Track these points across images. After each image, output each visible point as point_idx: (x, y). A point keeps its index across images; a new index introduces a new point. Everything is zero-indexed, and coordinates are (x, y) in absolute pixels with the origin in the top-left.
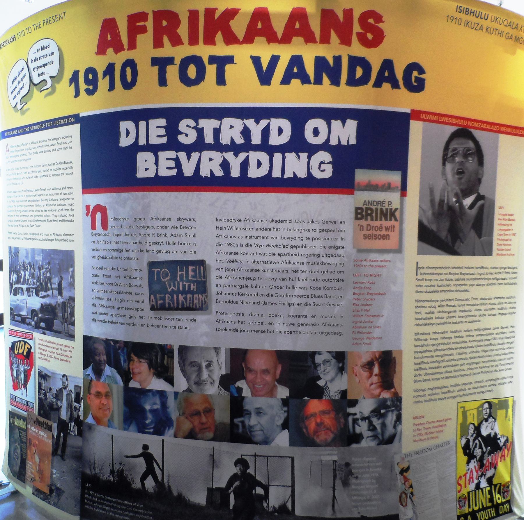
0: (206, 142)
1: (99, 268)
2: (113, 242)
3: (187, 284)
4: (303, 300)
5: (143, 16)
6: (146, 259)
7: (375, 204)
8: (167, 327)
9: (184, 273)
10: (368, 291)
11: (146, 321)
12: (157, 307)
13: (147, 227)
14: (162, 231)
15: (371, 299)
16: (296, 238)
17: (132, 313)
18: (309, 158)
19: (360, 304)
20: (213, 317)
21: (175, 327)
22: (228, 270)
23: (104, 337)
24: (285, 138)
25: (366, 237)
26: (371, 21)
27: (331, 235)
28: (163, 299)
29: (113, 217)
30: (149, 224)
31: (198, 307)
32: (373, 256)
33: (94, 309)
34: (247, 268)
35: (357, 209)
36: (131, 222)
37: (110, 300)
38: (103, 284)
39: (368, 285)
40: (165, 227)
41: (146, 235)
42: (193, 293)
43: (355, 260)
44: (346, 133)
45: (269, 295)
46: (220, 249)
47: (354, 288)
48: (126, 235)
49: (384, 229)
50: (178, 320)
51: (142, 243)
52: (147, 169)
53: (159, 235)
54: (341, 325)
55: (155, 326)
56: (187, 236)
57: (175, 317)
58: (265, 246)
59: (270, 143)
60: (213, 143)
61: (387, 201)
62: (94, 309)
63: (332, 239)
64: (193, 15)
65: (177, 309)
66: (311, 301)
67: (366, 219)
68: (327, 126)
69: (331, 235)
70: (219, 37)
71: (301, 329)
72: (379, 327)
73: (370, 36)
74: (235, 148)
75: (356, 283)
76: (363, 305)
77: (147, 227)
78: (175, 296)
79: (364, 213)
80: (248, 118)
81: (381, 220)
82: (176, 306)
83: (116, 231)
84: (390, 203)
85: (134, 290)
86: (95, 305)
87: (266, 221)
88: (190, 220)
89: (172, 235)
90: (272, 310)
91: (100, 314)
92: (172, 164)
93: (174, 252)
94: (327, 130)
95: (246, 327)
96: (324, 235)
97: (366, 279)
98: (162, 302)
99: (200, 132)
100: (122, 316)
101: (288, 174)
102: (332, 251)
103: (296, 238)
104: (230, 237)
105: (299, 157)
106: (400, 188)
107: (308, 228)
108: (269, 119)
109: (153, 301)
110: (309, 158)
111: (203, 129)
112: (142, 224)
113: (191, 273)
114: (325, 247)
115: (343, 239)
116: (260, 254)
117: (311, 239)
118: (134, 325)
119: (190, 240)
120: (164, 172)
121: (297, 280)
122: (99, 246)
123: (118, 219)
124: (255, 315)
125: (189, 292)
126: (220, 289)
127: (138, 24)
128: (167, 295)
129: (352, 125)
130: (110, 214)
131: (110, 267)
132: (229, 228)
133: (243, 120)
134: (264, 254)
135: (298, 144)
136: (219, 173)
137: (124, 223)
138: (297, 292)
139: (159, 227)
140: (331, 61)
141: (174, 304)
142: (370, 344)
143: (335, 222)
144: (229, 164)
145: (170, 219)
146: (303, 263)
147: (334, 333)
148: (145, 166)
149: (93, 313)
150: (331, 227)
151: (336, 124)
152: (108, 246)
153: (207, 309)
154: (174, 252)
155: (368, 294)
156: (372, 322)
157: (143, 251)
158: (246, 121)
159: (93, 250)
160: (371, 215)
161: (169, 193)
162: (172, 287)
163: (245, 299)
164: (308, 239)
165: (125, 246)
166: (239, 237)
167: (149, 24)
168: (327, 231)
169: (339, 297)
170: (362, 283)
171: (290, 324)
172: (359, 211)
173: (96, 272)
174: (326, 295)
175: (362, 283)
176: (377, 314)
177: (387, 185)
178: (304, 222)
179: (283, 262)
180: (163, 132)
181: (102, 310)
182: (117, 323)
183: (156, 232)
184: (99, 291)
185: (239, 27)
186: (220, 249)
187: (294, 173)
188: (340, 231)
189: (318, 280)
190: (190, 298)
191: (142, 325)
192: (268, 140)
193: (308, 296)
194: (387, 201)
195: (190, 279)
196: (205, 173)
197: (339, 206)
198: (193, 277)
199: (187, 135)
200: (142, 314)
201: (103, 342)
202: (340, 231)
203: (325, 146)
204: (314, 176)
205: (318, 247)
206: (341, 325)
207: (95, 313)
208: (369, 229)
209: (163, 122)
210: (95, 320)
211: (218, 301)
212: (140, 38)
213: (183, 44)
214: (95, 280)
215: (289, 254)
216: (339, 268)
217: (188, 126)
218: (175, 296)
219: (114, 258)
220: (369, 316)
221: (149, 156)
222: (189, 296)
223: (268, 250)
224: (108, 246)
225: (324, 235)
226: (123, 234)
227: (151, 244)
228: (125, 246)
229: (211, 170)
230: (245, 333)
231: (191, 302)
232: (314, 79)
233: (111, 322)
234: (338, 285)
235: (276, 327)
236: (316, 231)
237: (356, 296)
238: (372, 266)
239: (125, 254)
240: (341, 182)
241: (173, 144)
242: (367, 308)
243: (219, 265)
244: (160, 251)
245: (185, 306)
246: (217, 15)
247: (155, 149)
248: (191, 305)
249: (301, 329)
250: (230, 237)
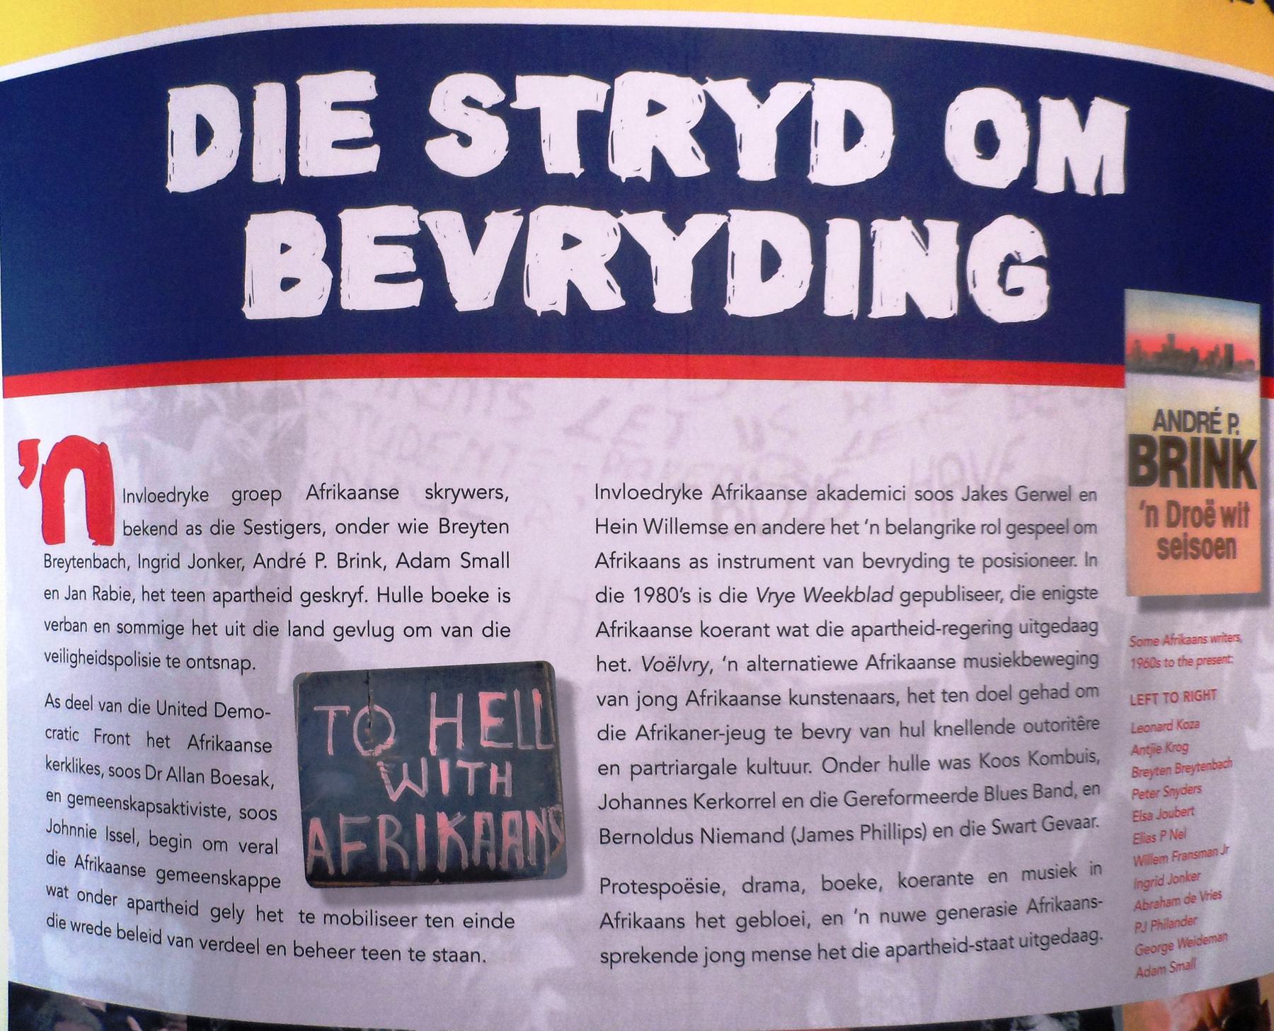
0: (550, 170)
1: (74, 704)
2: (137, 593)
3: (471, 767)
4: (953, 815)
6: (287, 664)
7: (1190, 423)
8: (385, 955)
9: (458, 721)
10: (1178, 757)
11: (289, 931)
12: (338, 869)
13: (292, 530)
14: (354, 545)
15: (1189, 790)
16: (921, 561)
17: (225, 896)
18: (964, 241)
19: (1156, 814)
20: (584, 905)
21: (419, 956)
22: (647, 701)
23: (99, 997)
24: (871, 158)
25: (1170, 550)
27: (1052, 546)
28: (367, 834)
29: (136, 488)
30: (298, 518)
31: (520, 863)
32: (1193, 622)
33: (56, 876)
34: (728, 691)
35: (1136, 441)
36: (219, 504)
37: (126, 838)
38: (92, 770)
39: (1176, 736)
40: (377, 528)
41: (286, 562)
42: (498, 805)
43: (1135, 642)
44: (1089, 148)
45: (824, 801)
46: (612, 613)
47: (1136, 751)
48: (197, 563)
49: (1219, 519)
50: (435, 922)
51: (270, 597)
52: (288, 284)
53: (343, 561)
54: (1094, 903)
55: (331, 953)
56: (468, 562)
57: (424, 910)
58: (800, 597)
59: (815, 177)
60: (578, 171)
61: (1225, 412)
62: (56, 876)
63: (1053, 562)
65: (430, 876)
66: (985, 814)
67: (1165, 483)
68: (1023, 118)
69: (1052, 546)
71: (950, 932)
72: (1217, 896)
74: (669, 195)
75: (1141, 729)
76: (1165, 815)
77: (292, 530)
78: (420, 820)
79: (1157, 459)
80: (723, 74)
81: (1209, 484)
82: (422, 863)
83: (150, 547)
84: (1234, 420)
85: (235, 798)
86: (62, 861)
87: (802, 495)
88: (481, 493)
89: (402, 561)
90: (835, 860)
91: (83, 896)
92: (403, 259)
93: (413, 631)
94: (1025, 134)
95: (727, 939)
96: (1025, 545)
97: (1172, 713)
98: (360, 846)
99: (524, 128)
100: (178, 909)
101: (887, 306)
102: (1053, 611)
103: (921, 561)
104: (656, 564)
105: (924, 234)
106: (1257, 366)
107: (965, 521)
108: (807, 79)
109: (318, 846)
110: (964, 241)
111: (534, 114)
112: (271, 514)
113: (488, 721)
114: (1030, 595)
115: (1091, 560)
116: (783, 632)
117: (978, 565)
118: (237, 947)
119: (481, 579)
120: (363, 295)
121: (930, 730)
122: (74, 611)
123: (160, 497)
124: (768, 888)
125: (482, 800)
126: (613, 786)
128: (382, 819)
129: (1110, 117)
130: (125, 477)
131: (126, 701)
132: (652, 526)
133: (702, 81)
134: (799, 631)
135: (919, 185)
136: (604, 296)
137: (189, 514)
138: (931, 781)
139: (343, 529)
141: (413, 855)
142: (1191, 965)
143: (1063, 496)
144: (647, 258)
145: (392, 494)
146: (950, 664)
147: (1074, 938)
148: (281, 267)
149: (50, 891)
150: (1047, 515)
151: (1057, 112)
152: (118, 612)
153: (560, 868)
154: (413, 631)
155: (1180, 768)
156: (1195, 877)
157: (274, 631)
159: (53, 626)
160: (1176, 465)
161: (389, 383)
162: (406, 783)
163: (725, 820)
164: (967, 562)
165: (190, 613)
166: (695, 563)
168: (1035, 530)
169: (1087, 790)
170: (1160, 728)
171: (907, 917)
172: (1143, 450)
173: (63, 718)
174: (1038, 788)
175: (1160, 728)
176: (1207, 846)
177: (1222, 353)
178: (948, 495)
179: (872, 662)
180: (360, 125)
181: (87, 880)
182: (157, 939)
183: (332, 545)
184: (75, 801)
186: (612, 613)
187: (909, 300)
188: (1082, 529)
189: (1008, 728)
190: (486, 828)
191: (270, 950)
192: (805, 166)
193: (973, 797)
194: (1225, 412)
195: (485, 744)
196: (544, 296)
197: (1070, 432)
198: (495, 734)
199: (465, 140)
200: (269, 899)
201: (92, 1019)
202: (1082, 529)
203: (1021, 198)
205: (1005, 594)
206: (1094, 903)
207: (61, 893)
208: (1174, 518)
209: (361, 84)
210: (62, 924)
211: (607, 837)
214: (61, 751)
215: (897, 627)
216: (1082, 676)
217: (470, 102)
218: (420, 820)
219: (145, 662)
220: (1186, 857)
221: (301, 228)
222: (481, 818)
223: (815, 614)
224: (118, 612)
225: (1025, 545)
226: (186, 560)
227: (310, 598)
228: (190, 613)
229: (571, 286)
230: (728, 967)
231: (491, 843)
233: (129, 935)
234: (1078, 742)
235: (855, 933)
236: (998, 529)
237: (1142, 784)
238: (1189, 662)
239: (193, 646)
240: (1077, 342)
241: (405, 171)
242: (1176, 824)
243: (611, 683)
244: (350, 631)
245: (465, 863)
247: (325, 199)
248: (491, 857)
249: (950, 932)
250: (656, 564)
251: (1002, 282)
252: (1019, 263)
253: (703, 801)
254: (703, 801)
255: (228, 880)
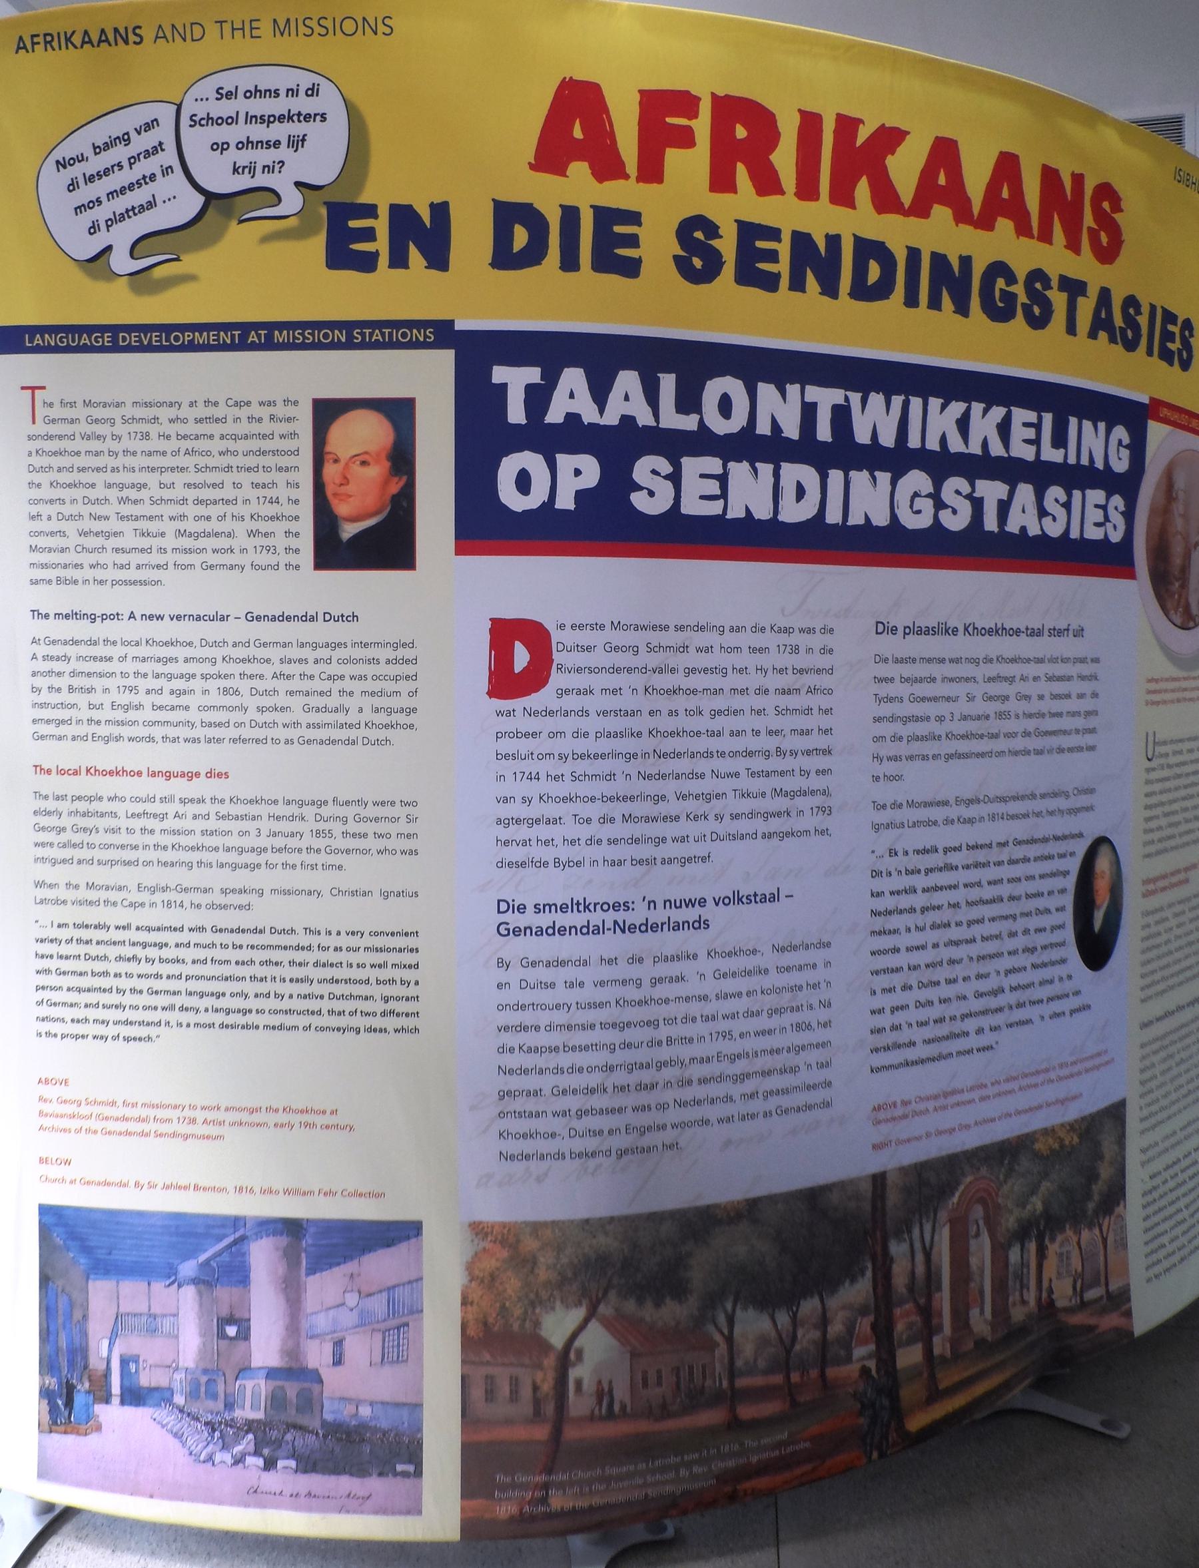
5: (685, 102)
26: (699, 235)
64: (810, 123)
70: (863, 190)
73: (697, 263)
99: (977, 504)
101: (856, 519)
105: (755, 470)
110: (894, 483)
127: (669, 120)
140: (426, 216)
158: (848, 393)
167: (702, 126)
185: (905, 168)
199: (651, 494)
204: (910, 527)
212: (673, 156)
213: (781, 192)
217: (654, 472)
232: (941, 295)
246: (863, 134)
251: (911, 507)
252: (919, 496)
253: (525, 1048)
254: (525, 1048)
255: (1000, 1010)
